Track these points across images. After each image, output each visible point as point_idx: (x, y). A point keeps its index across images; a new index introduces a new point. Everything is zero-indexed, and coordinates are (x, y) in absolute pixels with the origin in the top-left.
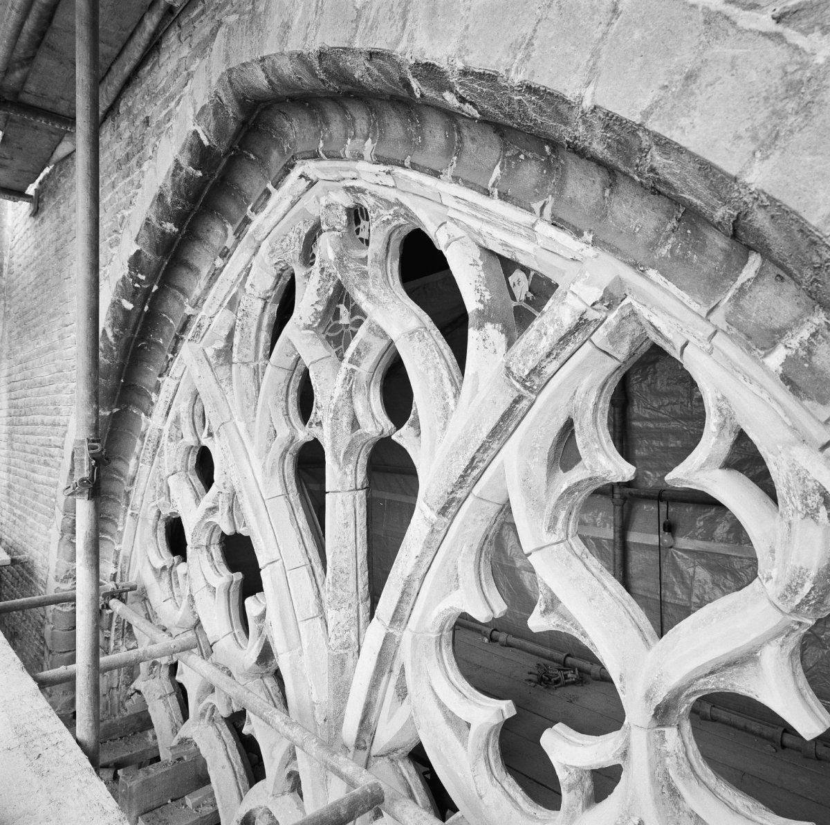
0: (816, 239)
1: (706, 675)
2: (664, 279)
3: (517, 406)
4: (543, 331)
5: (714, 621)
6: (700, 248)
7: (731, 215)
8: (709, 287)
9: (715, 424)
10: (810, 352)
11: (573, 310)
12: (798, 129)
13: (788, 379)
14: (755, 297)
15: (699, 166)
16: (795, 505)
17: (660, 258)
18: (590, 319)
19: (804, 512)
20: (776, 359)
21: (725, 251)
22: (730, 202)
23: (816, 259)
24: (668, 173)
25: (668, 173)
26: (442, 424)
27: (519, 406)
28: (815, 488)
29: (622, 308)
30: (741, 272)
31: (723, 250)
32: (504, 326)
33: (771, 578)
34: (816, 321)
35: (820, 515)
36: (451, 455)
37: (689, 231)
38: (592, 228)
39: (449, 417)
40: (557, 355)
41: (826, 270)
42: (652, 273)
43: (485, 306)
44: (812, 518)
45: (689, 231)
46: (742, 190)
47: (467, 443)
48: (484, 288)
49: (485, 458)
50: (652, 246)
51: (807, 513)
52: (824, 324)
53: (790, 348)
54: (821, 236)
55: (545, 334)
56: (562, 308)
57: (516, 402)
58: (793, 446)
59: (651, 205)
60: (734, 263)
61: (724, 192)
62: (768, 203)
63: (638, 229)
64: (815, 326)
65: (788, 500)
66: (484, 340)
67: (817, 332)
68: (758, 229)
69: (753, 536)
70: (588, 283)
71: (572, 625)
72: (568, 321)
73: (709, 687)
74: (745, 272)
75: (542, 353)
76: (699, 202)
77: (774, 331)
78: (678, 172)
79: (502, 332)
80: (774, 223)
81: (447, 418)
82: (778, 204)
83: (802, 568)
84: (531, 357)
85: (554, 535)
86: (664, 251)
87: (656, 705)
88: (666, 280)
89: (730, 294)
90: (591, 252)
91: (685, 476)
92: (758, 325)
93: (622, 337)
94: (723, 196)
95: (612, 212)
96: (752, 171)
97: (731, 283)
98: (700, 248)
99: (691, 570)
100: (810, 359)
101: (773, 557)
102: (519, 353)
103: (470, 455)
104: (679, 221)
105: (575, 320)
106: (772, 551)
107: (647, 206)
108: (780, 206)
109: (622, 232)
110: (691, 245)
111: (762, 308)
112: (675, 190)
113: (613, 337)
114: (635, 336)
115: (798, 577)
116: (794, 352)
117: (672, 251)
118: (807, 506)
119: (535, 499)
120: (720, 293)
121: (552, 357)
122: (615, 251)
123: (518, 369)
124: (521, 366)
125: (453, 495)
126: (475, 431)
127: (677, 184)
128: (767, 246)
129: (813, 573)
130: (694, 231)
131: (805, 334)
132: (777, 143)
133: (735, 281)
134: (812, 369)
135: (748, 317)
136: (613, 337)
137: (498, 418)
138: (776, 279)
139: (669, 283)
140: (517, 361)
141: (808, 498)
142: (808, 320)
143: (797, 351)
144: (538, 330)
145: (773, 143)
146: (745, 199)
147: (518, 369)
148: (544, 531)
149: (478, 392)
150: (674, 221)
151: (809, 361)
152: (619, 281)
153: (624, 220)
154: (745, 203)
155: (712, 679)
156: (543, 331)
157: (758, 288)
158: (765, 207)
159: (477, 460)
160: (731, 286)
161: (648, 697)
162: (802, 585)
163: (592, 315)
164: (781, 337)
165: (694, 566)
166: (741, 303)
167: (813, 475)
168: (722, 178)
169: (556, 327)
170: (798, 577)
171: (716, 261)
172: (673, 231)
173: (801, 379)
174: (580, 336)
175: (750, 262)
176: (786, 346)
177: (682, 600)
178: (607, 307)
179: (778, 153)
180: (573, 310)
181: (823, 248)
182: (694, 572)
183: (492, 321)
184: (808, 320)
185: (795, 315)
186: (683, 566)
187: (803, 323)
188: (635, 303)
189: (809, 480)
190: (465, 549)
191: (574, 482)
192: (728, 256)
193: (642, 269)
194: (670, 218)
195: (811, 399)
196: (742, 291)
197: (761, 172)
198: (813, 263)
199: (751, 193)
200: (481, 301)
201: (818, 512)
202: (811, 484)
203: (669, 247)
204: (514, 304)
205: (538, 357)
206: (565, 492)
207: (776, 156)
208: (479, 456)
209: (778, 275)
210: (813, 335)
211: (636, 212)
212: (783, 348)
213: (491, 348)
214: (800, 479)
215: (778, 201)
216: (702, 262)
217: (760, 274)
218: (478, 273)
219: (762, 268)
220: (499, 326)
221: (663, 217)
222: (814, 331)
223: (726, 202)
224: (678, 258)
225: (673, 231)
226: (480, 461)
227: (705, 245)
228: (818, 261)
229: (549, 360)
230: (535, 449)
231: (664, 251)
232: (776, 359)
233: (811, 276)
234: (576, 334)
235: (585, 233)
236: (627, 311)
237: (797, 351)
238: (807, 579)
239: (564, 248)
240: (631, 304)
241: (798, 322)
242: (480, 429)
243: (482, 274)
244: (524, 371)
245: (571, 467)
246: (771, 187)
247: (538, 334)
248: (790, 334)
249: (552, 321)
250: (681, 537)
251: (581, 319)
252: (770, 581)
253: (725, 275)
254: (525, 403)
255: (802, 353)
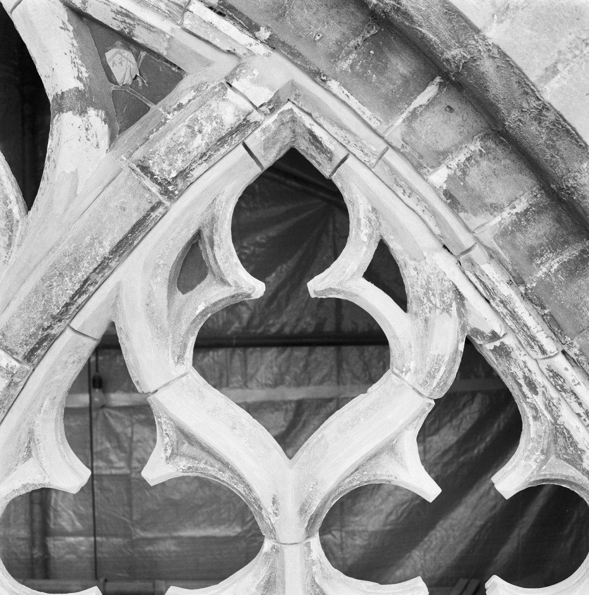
0: (529, 91)
1: (352, 473)
2: (346, 92)
3: (152, 214)
4: (196, 128)
5: (362, 420)
6: (381, 70)
7: (464, 56)
8: (386, 106)
9: (366, 234)
10: (464, 173)
11: (237, 108)
12: (521, 7)
13: (450, 194)
14: (424, 121)
15: (445, 11)
16: (434, 303)
17: (341, 71)
18: (251, 121)
19: (442, 308)
20: (440, 177)
21: (405, 77)
22: (466, 47)
23: (525, 105)
24: (412, 7)
25: (412, 7)
26: (6, 239)
27: (153, 215)
28: (450, 287)
29: (282, 113)
30: (415, 98)
31: (403, 76)
32: (107, 114)
33: (410, 370)
34: (472, 148)
35: (452, 308)
36: (50, 278)
37: (372, 52)
38: (269, 25)
39: (14, 229)
40: (210, 157)
41: (530, 115)
42: (334, 85)
43: (84, 85)
44: (447, 312)
45: (372, 52)
46: (480, 41)
47: (77, 261)
48: (80, 62)
49: (98, 279)
50: (334, 57)
51: (444, 308)
52: (478, 151)
53: (451, 168)
54: (535, 90)
55: (200, 132)
56: (222, 104)
57: (153, 209)
58: (436, 252)
59: (337, 17)
60: (411, 88)
61: (463, 38)
62: (498, 56)
63: (318, 38)
64: (470, 152)
65: (425, 300)
66: (87, 129)
67: (471, 157)
68: (483, 73)
69: (395, 337)
70: (257, 82)
71: (206, 463)
72: (230, 119)
73: (355, 484)
74: (419, 98)
75: (195, 153)
76: (434, 38)
77: (439, 153)
78: (424, 9)
79: (105, 122)
80: (498, 71)
81: (12, 231)
82: (507, 59)
83: (439, 355)
84: (180, 157)
85: (183, 366)
86: (345, 65)
87: (310, 515)
88: (349, 94)
89: (404, 116)
90: (261, 49)
91: (338, 286)
92: (428, 147)
93: (274, 144)
94: (461, 40)
95: (291, 14)
96: (491, 29)
97: (406, 106)
98: (381, 70)
99: (129, 430)
100: (464, 178)
101: (411, 351)
102: (163, 150)
103: (81, 275)
104: (365, 40)
105: (239, 120)
106: (410, 347)
107: (332, 18)
108: (508, 61)
109: (301, 37)
110: (371, 65)
111: (430, 132)
112: (413, 22)
113: (268, 143)
114: (285, 143)
115: (436, 363)
116: (453, 172)
117: (352, 66)
118: (444, 302)
119: (159, 326)
120: (397, 113)
121: (204, 158)
122: (293, 55)
123: (162, 170)
124: (165, 166)
125: (49, 331)
126: (91, 245)
127: (417, 17)
128: (485, 87)
129: (446, 359)
130: (378, 53)
131: (462, 158)
132: (508, 13)
133: (409, 105)
134: (465, 187)
135: (419, 138)
136: (268, 143)
137: (128, 229)
138: (445, 109)
139: (351, 97)
140: (159, 160)
141: (445, 295)
142: (466, 147)
143: (455, 171)
144: (189, 126)
145: (506, 12)
146: (480, 48)
147: (162, 170)
148: (171, 362)
149: (76, 195)
150: (360, 40)
151: (464, 180)
152: (293, 86)
153: (304, 25)
154: (480, 51)
155: (357, 475)
156: (196, 128)
157: (427, 114)
158: (494, 58)
159: (89, 282)
160: (406, 109)
161: (302, 511)
162: (439, 370)
163: (256, 116)
164: (444, 159)
165: (132, 425)
166: (413, 125)
167: (449, 276)
168: (465, 27)
169: (214, 124)
170: (436, 363)
171: (394, 84)
172: (356, 48)
173: (460, 195)
174: (237, 138)
175: (426, 91)
176: (448, 166)
177: (120, 468)
178: (270, 110)
179: (509, 21)
180: (237, 108)
181: (533, 98)
182: (132, 432)
183: (96, 107)
184: (466, 147)
185: (456, 142)
186: (119, 429)
187: (461, 148)
188: (296, 110)
189: (445, 281)
190: (47, 403)
191: (213, 301)
192: (406, 81)
193: (324, 78)
194: (356, 36)
195: (466, 211)
196: (414, 115)
197: (498, 32)
198: (523, 108)
199: (486, 45)
200: (79, 79)
201: (451, 306)
202: (447, 284)
203: (349, 62)
204: (113, 87)
205: (190, 157)
206: (200, 314)
207: (507, 23)
208: (94, 276)
209: (449, 107)
210: (468, 159)
211: (319, 21)
212: (445, 168)
213: (94, 140)
214: (439, 280)
215: (508, 57)
216: (380, 82)
217: (432, 103)
218: (70, 41)
219: (435, 98)
220: (102, 113)
221: (348, 32)
222: (469, 156)
223: (462, 45)
224: (358, 75)
225: (356, 48)
226: (91, 284)
227: (386, 67)
228: (527, 107)
229: (200, 162)
230: (159, 266)
231: (345, 65)
232: (440, 177)
233: (517, 116)
234: (234, 136)
235: (262, 29)
236: (288, 117)
237: (455, 171)
238: (443, 364)
239: (226, 37)
240: (292, 110)
241: (458, 147)
242: (100, 243)
243: (75, 42)
244: (170, 173)
245: (192, 287)
246: (504, 45)
247: (189, 130)
248: (450, 156)
249: (209, 118)
250: (114, 391)
251: (244, 120)
252: (409, 373)
253: (400, 98)
254: (161, 210)
255: (459, 173)
